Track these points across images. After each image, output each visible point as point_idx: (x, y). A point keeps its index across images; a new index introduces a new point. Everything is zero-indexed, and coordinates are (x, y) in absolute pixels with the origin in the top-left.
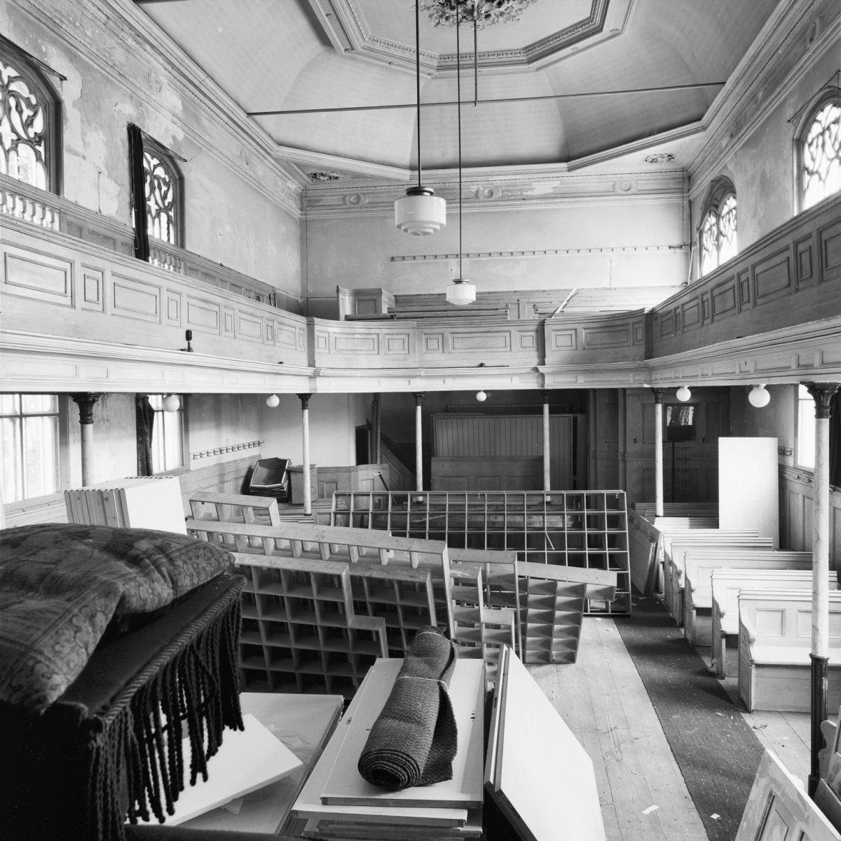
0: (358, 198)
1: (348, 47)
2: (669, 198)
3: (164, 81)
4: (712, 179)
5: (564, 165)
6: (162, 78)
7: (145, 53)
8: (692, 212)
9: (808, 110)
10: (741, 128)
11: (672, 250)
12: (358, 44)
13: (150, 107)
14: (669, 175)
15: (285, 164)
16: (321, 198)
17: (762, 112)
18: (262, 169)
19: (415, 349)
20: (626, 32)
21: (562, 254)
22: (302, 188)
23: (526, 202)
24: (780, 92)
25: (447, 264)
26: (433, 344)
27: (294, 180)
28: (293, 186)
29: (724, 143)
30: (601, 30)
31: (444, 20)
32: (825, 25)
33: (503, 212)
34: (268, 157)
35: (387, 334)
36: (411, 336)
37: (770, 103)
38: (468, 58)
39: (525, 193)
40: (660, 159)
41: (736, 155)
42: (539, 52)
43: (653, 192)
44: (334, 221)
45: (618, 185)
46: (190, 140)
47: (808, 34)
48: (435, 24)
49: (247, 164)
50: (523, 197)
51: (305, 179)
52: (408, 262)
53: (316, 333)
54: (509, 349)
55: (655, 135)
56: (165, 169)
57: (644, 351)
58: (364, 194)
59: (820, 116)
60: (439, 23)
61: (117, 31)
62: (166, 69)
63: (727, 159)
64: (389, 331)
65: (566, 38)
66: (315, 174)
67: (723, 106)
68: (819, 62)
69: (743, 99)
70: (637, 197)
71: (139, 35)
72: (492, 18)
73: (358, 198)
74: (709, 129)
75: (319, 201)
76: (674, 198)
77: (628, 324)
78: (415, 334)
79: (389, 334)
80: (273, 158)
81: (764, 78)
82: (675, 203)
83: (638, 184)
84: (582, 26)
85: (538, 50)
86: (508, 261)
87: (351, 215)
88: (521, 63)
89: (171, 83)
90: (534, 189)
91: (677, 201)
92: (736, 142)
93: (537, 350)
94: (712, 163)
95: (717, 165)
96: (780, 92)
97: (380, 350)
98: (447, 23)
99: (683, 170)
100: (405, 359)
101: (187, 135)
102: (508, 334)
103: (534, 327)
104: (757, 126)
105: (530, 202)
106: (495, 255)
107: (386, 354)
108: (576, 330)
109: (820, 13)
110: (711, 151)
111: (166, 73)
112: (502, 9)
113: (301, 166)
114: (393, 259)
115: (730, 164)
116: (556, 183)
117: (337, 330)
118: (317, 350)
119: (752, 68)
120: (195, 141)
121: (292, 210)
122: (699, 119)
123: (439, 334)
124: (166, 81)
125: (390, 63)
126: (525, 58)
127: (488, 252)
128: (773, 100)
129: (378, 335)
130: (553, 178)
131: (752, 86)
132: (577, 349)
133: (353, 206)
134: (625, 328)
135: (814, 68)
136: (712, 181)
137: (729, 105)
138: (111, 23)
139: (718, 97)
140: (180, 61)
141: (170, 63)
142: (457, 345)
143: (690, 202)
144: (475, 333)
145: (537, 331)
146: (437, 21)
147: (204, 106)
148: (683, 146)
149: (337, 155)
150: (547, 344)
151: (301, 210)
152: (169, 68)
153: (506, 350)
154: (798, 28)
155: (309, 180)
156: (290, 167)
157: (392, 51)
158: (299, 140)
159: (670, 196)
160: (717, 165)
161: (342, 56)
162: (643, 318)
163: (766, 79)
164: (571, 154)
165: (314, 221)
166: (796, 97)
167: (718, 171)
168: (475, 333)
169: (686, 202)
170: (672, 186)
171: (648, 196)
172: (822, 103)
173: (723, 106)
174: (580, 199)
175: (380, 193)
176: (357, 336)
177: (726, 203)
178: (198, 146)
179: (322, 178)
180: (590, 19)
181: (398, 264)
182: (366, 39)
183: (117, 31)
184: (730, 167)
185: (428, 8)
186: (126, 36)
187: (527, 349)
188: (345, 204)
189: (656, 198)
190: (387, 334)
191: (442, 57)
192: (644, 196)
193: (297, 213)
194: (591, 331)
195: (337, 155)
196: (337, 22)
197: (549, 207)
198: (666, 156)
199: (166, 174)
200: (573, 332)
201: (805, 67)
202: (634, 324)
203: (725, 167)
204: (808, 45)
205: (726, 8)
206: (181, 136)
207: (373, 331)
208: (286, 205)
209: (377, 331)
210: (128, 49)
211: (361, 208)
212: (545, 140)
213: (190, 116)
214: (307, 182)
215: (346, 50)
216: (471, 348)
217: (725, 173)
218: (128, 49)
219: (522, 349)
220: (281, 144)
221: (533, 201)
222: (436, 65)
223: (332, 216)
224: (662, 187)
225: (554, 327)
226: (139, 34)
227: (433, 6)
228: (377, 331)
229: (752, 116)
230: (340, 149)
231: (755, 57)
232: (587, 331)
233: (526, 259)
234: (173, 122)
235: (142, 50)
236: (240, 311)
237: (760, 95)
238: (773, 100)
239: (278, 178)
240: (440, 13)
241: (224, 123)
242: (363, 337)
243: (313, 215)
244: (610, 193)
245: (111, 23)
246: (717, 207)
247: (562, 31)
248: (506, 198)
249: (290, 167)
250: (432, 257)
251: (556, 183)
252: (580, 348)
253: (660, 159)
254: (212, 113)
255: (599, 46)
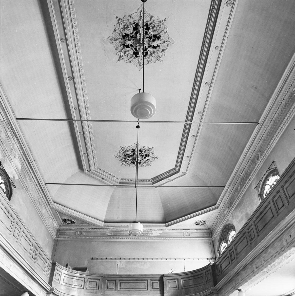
0: (81, 233)
1: (89, 169)
2: (205, 239)
3: (17, 155)
4: (222, 227)
5: (164, 225)
6: (16, 154)
7: (13, 141)
8: (214, 245)
9: (262, 181)
10: (232, 204)
11: (208, 260)
12: (93, 169)
13: (8, 160)
14: (203, 231)
15: (54, 212)
16: (66, 232)
17: (242, 192)
18: (45, 210)
19: (102, 287)
20: (187, 174)
21: (164, 260)
22: (59, 227)
23: (149, 238)
24: (248, 182)
25: (116, 262)
26: (111, 286)
27: (56, 222)
28: (55, 225)
29: (225, 212)
30: (179, 172)
31: (125, 163)
32: (262, 154)
33: (140, 242)
34: (48, 206)
35: (89, 279)
36: (100, 280)
37: (245, 188)
38: (131, 180)
39: (149, 235)
40: (200, 223)
41: (232, 214)
42: (156, 180)
43: (198, 237)
44: (70, 241)
45: (185, 234)
46: (20, 182)
47: (256, 159)
48: (121, 164)
49: (40, 205)
50: (148, 236)
51: (60, 221)
52: (99, 260)
53: (56, 271)
54: (146, 289)
55: (199, 211)
56: (5, 186)
57: (213, 284)
58: (84, 231)
59: (268, 183)
60: (123, 164)
61: (6, 127)
62: (19, 151)
63: (228, 217)
64: (91, 277)
65: (166, 175)
66: (65, 220)
67: (224, 197)
68: (263, 165)
69: (232, 192)
70: (193, 238)
71: (14, 132)
72: (142, 164)
73: (81, 233)
74: (219, 208)
75: (64, 233)
76: (207, 239)
77: (202, 274)
78: (102, 280)
79: (90, 279)
80: (50, 208)
81: (240, 181)
82: (206, 242)
83: (192, 234)
84: (172, 171)
85: (156, 180)
86: (142, 262)
87: (77, 239)
88: (150, 184)
89: (19, 157)
90: (153, 233)
91: (208, 241)
92: (231, 209)
93: (160, 290)
94: (221, 222)
95: (224, 221)
96: (248, 182)
97: (85, 286)
98: (126, 164)
99: (209, 229)
100: (96, 293)
101: (19, 179)
102: (147, 281)
103: (158, 278)
104: (240, 199)
105: (151, 238)
106: (136, 259)
107: (87, 289)
108: (178, 279)
109: (259, 150)
110: (220, 218)
111: (19, 152)
112: (146, 159)
113: (61, 213)
114: (92, 259)
115: (230, 218)
116: (161, 232)
117: (66, 272)
118: (54, 279)
119: (235, 178)
120: (22, 183)
121: (53, 234)
122: (215, 204)
123: (114, 280)
124: (18, 156)
125: (102, 179)
126: (151, 182)
127: (134, 258)
128: (246, 186)
129: (85, 278)
130: (158, 230)
131: (236, 186)
132: (179, 289)
133: (79, 236)
134: (201, 276)
135: (261, 167)
136: (223, 228)
137: (227, 195)
138: (4, 123)
139: (222, 194)
140: (26, 150)
141: (22, 149)
142: (122, 287)
143: (213, 242)
144: (131, 280)
145: (159, 280)
146: (122, 163)
147: (30, 173)
148: (208, 216)
149: (76, 211)
150: (165, 286)
151: (56, 235)
152: (21, 151)
153: (145, 289)
154: (252, 158)
155: (62, 223)
156: (57, 213)
157: (104, 174)
158: (63, 203)
159: (206, 239)
160: (224, 221)
161: (86, 174)
162: (210, 268)
163: (241, 182)
164: (167, 220)
165: (61, 241)
166: (256, 180)
167: (225, 223)
168: (131, 280)
169: (211, 241)
170: (205, 235)
171: (196, 238)
172: (267, 177)
173: (224, 197)
174: (171, 238)
175: (90, 231)
176: (74, 278)
177: (230, 235)
178: (22, 186)
179: (68, 222)
180: (175, 168)
181: (94, 261)
182: (96, 167)
183: (6, 127)
184: (230, 219)
185: (120, 157)
186: (8, 130)
187: (155, 290)
188: (75, 234)
189: (200, 239)
190: (89, 279)
191: (122, 179)
192: (195, 238)
193: (54, 236)
194: (185, 279)
195: (76, 211)
196: (87, 158)
197: (159, 241)
198: (203, 221)
199: (5, 188)
200: (176, 280)
201: (257, 169)
202: (205, 272)
203: (228, 220)
204: (257, 161)
205: (223, 161)
206: (17, 178)
207: (83, 276)
208: (51, 231)
209: (85, 276)
210: (8, 136)
211: (82, 236)
212: (157, 215)
213: (22, 173)
214: (62, 224)
215: (88, 171)
216: (129, 288)
217: (228, 223)
218: (8, 136)
219: (153, 289)
220: (55, 202)
221: (152, 238)
222: (119, 182)
223: (70, 239)
224: (201, 235)
225: (168, 278)
226: (14, 132)
227: (122, 156)
228: (85, 276)
229: (236, 197)
230: (78, 209)
231: (236, 173)
232: (183, 279)
233: (149, 262)
234: (15, 171)
235: (12, 139)
236: (23, 232)
237: (239, 188)
238: (246, 186)
239: (50, 218)
240: (124, 159)
241: (35, 184)
242: (77, 278)
243: (62, 238)
244: (183, 236)
245: (4, 123)
246: (226, 238)
247: (165, 173)
248: (141, 236)
249: (57, 213)
250: (109, 259)
251: (161, 232)
252: (180, 288)
253: (200, 223)
254: (32, 177)
255: (178, 179)
